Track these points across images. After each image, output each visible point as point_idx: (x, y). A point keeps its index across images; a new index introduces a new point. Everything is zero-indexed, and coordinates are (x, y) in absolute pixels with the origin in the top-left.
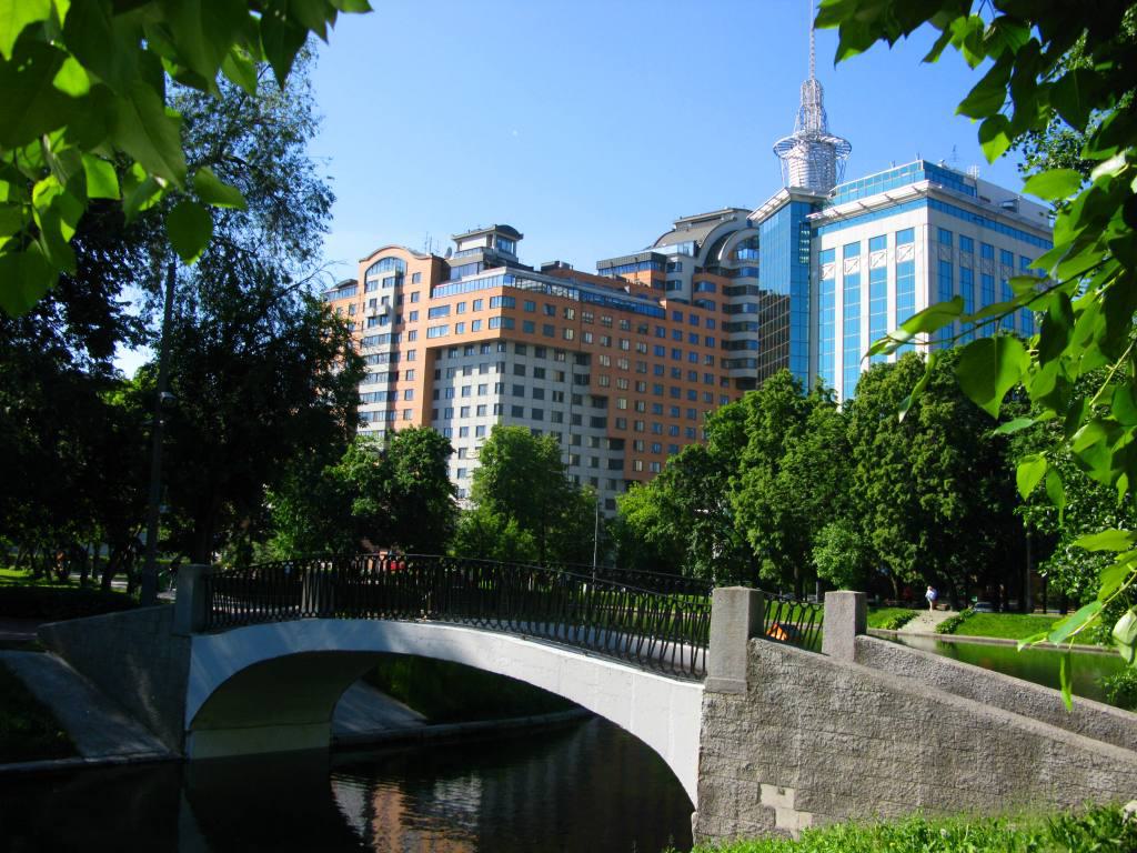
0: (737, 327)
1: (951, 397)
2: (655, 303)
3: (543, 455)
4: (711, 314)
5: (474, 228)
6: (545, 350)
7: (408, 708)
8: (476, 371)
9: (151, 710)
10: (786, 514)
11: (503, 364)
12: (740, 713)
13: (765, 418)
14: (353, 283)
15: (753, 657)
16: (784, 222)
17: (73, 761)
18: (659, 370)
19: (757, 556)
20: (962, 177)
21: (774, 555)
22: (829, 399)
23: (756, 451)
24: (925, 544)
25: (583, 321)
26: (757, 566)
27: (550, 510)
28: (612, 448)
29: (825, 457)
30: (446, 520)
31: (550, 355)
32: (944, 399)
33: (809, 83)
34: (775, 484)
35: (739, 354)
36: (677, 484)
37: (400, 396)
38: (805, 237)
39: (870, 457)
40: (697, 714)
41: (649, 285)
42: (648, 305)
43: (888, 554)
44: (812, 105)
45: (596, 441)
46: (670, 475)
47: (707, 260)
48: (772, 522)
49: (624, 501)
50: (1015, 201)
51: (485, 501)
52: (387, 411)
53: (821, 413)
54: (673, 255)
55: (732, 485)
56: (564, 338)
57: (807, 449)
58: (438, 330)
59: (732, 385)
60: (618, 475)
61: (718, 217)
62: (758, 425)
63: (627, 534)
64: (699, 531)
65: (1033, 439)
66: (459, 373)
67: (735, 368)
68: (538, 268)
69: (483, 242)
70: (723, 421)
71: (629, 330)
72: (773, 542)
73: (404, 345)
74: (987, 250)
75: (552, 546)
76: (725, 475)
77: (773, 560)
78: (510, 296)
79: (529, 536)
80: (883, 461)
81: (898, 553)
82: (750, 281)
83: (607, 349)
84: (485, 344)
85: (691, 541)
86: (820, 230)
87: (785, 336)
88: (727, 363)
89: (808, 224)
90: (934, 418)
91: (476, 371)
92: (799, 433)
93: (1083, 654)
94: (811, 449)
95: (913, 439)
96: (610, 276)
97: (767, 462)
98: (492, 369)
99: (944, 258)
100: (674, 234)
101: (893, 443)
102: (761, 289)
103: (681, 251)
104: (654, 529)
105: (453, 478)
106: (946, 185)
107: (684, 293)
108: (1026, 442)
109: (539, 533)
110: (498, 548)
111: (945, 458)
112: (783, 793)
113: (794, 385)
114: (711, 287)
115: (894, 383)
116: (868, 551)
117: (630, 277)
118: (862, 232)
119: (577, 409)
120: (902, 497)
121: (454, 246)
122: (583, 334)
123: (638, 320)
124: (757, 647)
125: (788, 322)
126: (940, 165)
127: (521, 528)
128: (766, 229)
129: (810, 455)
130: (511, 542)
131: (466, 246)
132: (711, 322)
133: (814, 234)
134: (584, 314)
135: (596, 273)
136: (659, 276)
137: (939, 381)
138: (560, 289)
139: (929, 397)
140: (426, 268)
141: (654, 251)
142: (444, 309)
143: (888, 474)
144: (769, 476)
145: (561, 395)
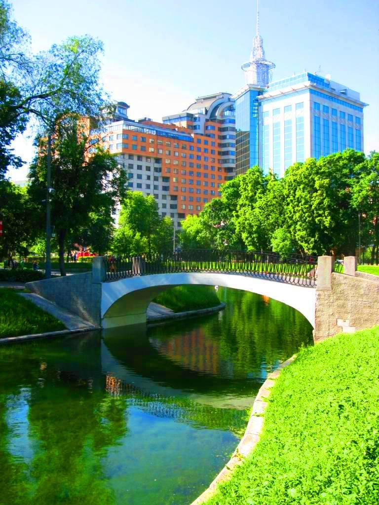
0: (224, 145)
4: (213, 140)
7: (165, 307)
9: (83, 311)
10: (259, 227)
12: (329, 297)
13: (248, 186)
15: (333, 279)
16: (247, 99)
17: (66, 331)
18: (191, 165)
21: (254, 244)
22: (275, 178)
24: (318, 238)
28: (171, 199)
29: (274, 202)
31: (144, 159)
32: (324, 177)
33: (256, 37)
38: (255, 106)
40: (315, 297)
41: (186, 127)
43: (302, 242)
44: (258, 47)
46: (206, 211)
47: (211, 116)
50: (345, 90)
53: (272, 184)
55: (234, 215)
60: (174, 211)
61: (215, 97)
64: (220, 235)
67: (224, 163)
70: (228, 188)
71: (178, 148)
72: (253, 238)
74: (334, 111)
76: (231, 211)
79: (146, 239)
80: (300, 204)
81: (307, 242)
82: (231, 125)
83: (169, 156)
86: (262, 103)
87: (247, 150)
88: (221, 161)
89: (257, 100)
90: (321, 186)
94: (269, 199)
96: (169, 124)
100: (196, 104)
101: (304, 196)
103: (199, 112)
106: (317, 83)
107: (201, 131)
108: (359, 195)
112: (345, 321)
116: (294, 242)
117: (177, 124)
118: (281, 104)
120: (308, 219)
122: (158, 150)
124: (334, 275)
125: (246, 144)
126: (314, 74)
127: (141, 236)
128: (238, 103)
129: (268, 202)
130: (138, 242)
133: (260, 105)
134: (158, 141)
135: (162, 122)
137: (322, 170)
138: (148, 130)
141: (188, 112)
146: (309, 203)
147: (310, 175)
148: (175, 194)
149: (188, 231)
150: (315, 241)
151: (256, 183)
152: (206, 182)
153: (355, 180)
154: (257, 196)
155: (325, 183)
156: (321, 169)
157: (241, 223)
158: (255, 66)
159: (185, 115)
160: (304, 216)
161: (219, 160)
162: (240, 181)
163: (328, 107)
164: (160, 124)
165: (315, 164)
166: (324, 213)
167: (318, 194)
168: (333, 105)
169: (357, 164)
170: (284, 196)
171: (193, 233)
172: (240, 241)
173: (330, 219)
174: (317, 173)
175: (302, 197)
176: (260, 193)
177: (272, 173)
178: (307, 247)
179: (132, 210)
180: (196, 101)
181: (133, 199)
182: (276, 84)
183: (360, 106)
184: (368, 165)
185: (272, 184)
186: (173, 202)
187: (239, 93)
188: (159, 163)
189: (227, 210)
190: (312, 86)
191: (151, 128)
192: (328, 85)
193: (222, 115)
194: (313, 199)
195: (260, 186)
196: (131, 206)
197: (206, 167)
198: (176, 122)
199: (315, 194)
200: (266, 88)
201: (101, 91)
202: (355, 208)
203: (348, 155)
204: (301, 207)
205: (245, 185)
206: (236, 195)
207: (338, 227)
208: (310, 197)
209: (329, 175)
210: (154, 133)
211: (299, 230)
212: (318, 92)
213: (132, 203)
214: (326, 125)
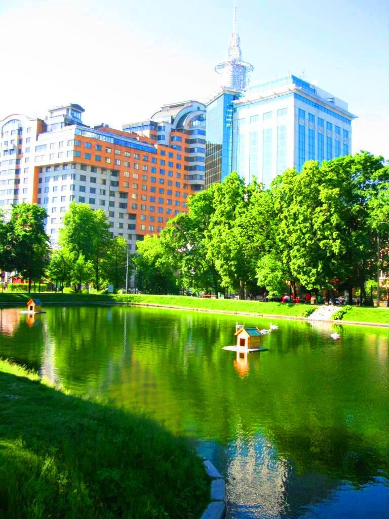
0: (192, 159)
2: (152, 146)
5: (59, 105)
6: (96, 168)
8: (60, 179)
11: (75, 175)
13: (225, 198)
16: (219, 105)
18: (154, 180)
23: (219, 216)
24: (322, 268)
28: (130, 218)
30: (44, 256)
31: (99, 171)
35: (193, 173)
37: (20, 191)
38: (229, 113)
43: (299, 273)
45: (121, 215)
48: (230, 256)
50: (332, 98)
51: (66, 245)
52: (14, 199)
55: (206, 235)
59: (189, 188)
60: (133, 232)
66: (52, 180)
68: (92, 127)
69: (64, 112)
71: (139, 159)
73: (22, 165)
74: (321, 121)
76: (201, 230)
77: (230, 278)
78: (79, 141)
79: (91, 264)
80: (297, 222)
81: (305, 273)
82: (200, 137)
84: (65, 165)
90: (329, 198)
91: (60, 179)
96: (129, 132)
98: (69, 178)
104: (159, 260)
105: (48, 233)
107: (166, 142)
109: (96, 262)
110: (74, 271)
111: (335, 219)
113: (240, 180)
114: (180, 139)
116: (287, 272)
117: (139, 133)
119: (112, 199)
120: (309, 242)
121: (49, 114)
125: (216, 158)
127: (86, 259)
128: (209, 109)
130: (80, 268)
131: (55, 114)
132: (179, 157)
133: (235, 110)
135: (122, 130)
137: (328, 177)
138: (104, 138)
140: (34, 126)
141: (152, 120)
145: (104, 191)
149: (144, 256)
150: (318, 273)
151: (235, 195)
152: (170, 201)
155: (334, 193)
157: (215, 245)
158: (230, 67)
159: (149, 123)
160: (304, 238)
162: (214, 192)
163: (313, 116)
164: (120, 131)
166: (332, 235)
167: (322, 209)
168: (318, 113)
169: (376, 170)
171: (151, 259)
172: (212, 268)
173: (341, 243)
176: (240, 208)
178: (306, 280)
179: (76, 227)
180: (161, 109)
181: (78, 214)
183: (347, 118)
185: (258, 195)
186: (132, 222)
187: (212, 98)
190: (296, 89)
193: (190, 124)
195: (240, 198)
196: (74, 222)
197: (170, 183)
198: (137, 131)
199: (318, 209)
200: (243, 92)
202: (374, 229)
204: (299, 225)
205: (221, 196)
206: (209, 210)
207: (349, 255)
211: (295, 257)
212: (303, 97)
213: (76, 218)
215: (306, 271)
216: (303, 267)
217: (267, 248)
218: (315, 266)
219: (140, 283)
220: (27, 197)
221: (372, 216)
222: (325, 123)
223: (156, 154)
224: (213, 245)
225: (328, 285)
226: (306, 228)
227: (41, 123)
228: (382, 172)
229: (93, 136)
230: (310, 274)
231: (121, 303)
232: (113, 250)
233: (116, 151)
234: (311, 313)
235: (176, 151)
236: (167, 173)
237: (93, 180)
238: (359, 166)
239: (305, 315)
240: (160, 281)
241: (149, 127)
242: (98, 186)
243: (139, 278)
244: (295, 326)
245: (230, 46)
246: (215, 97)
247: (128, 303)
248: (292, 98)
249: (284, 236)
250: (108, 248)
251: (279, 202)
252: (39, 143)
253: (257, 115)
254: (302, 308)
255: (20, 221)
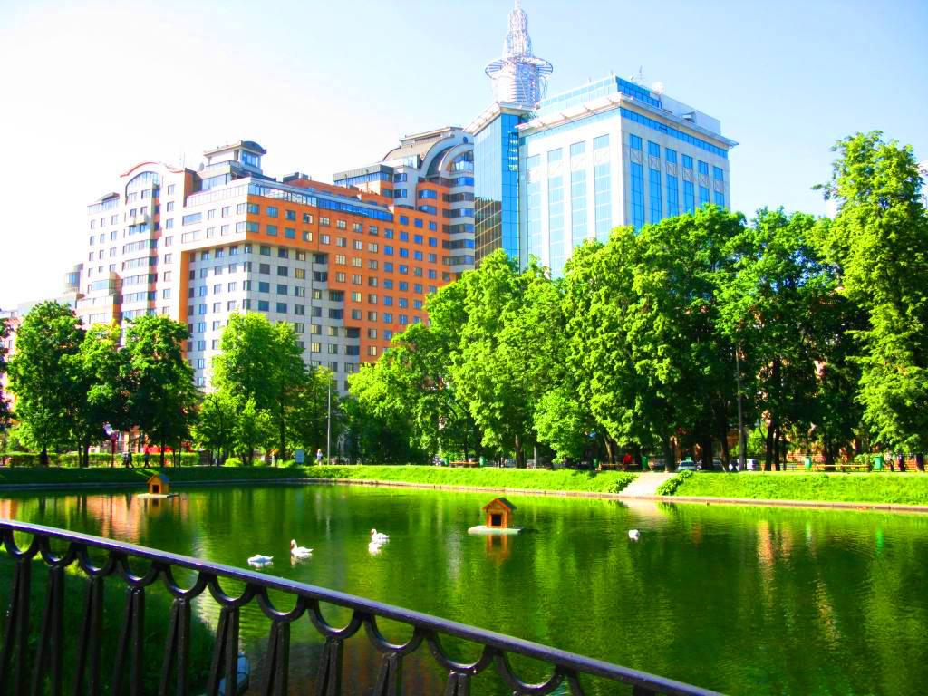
0: (456, 229)
1: (661, 267)
3: (280, 339)
5: (222, 145)
6: (287, 251)
8: (226, 270)
10: (507, 386)
11: (250, 264)
13: (483, 295)
14: (115, 196)
19: (479, 426)
20: (649, 92)
21: (494, 424)
23: (475, 326)
24: (641, 408)
25: (320, 225)
26: (480, 436)
27: (289, 391)
31: (292, 254)
32: (654, 269)
33: (515, 13)
34: (494, 357)
36: (402, 362)
37: (159, 295)
38: (513, 146)
39: (586, 327)
41: (379, 194)
42: (378, 211)
43: (605, 418)
48: (492, 393)
49: (356, 380)
50: (692, 114)
53: (537, 289)
54: (399, 167)
55: (453, 361)
56: (338, 281)
57: (524, 323)
58: (191, 235)
61: (438, 135)
62: (477, 303)
63: (360, 411)
65: (744, 304)
66: (211, 273)
67: (454, 264)
68: (280, 179)
69: (231, 156)
72: (493, 410)
73: (162, 250)
74: (672, 154)
75: (292, 424)
76: (447, 351)
77: (494, 430)
79: (267, 416)
80: (598, 330)
81: (615, 418)
84: (234, 246)
85: (416, 413)
90: (648, 288)
91: (226, 270)
92: (516, 308)
93: (793, 511)
94: (529, 322)
95: (627, 309)
96: (345, 186)
97: (486, 338)
98: (240, 268)
99: (636, 161)
102: (475, 196)
103: (406, 164)
107: (409, 200)
111: (659, 323)
113: (510, 264)
114: (433, 194)
115: (607, 255)
116: (586, 418)
117: (362, 187)
120: (618, 364)
121: (205, 161)
123: (368, 223)
125: (496, 222)
126: (630, 81)
127: (258, 407)
129: (527, 328)
130: (250, 422)
131: (215, 159)
132: (433, 226)
133: (522, 141)
135: (332, 183)
136: (388, 185)
137: (649, 252)
139: (641, 268)
140: (180, 181)
141: (384, 164)
142: (195, 217)
143: (604, 343)
144: (488, 349)
146: (620, 329)
147: (621, 264)
148: (354, 324)
153: (724, 273)
154: (502, 317)
155: (656, 279)
156: (645, 251)
161: (444, 258)
165: (631, 238)
167: (639, 306)
170: (563, 317)
174: (638, 260)
175: (602, 315)
177: (538, 265)
178: (616, 429)
180: (401, 144)
182: (555, 100)
184: (753, 239)
185: (537, 289)
187: (482, 121)
188: (323, 263)
189: (440, 350)
191: (306, 193)
192: (658, 102)
193: (451, 168)
194: (630, 317)
195: (509, 294)
196: (239, 344)
199: (632, 307)
200: (534, 110)
201: (507, 323)
202: (727, 337)
203: (707, 217)
207: (689, 382)
208: (622, 314)
209: (664, 263)
210: (314, 203)
211: (598, 391)
214: (656, 183)
215: (616, 414)
216: (612, 408)
217: (555, 379)
218: (631, 405)
219: (355, 446)
220: (169, 307)
221: (724, 316)
222: (679, 157)
223: (392, 221)
224: (464, 376)
225: (654, 436)
226: (612, 340)
227: (192, 176)
228: (739, 240)
229: (281, 196)
230: (623, 419)
231: (316, 480)
232: (310, 391)
233: (321, 218)
234: (626, 485)
235: (426, 215)
236: (412, 256)
237: (283, 271)
238: (701, 232)
239: (614, 489)
240: (388, 441)
241: (379, 176)
242: (291, 281)
243: (352, 438)
244: (598, 507)
245: (511, 32)
246: (493, 115)
247: (326, 480)
248: (617, 119)
249: (579, 356)
250: (301, 387)
251: (572, 298)
252: (190, 210)
253: (560, 148)
254: (612, 477)
255: (139, 346)
